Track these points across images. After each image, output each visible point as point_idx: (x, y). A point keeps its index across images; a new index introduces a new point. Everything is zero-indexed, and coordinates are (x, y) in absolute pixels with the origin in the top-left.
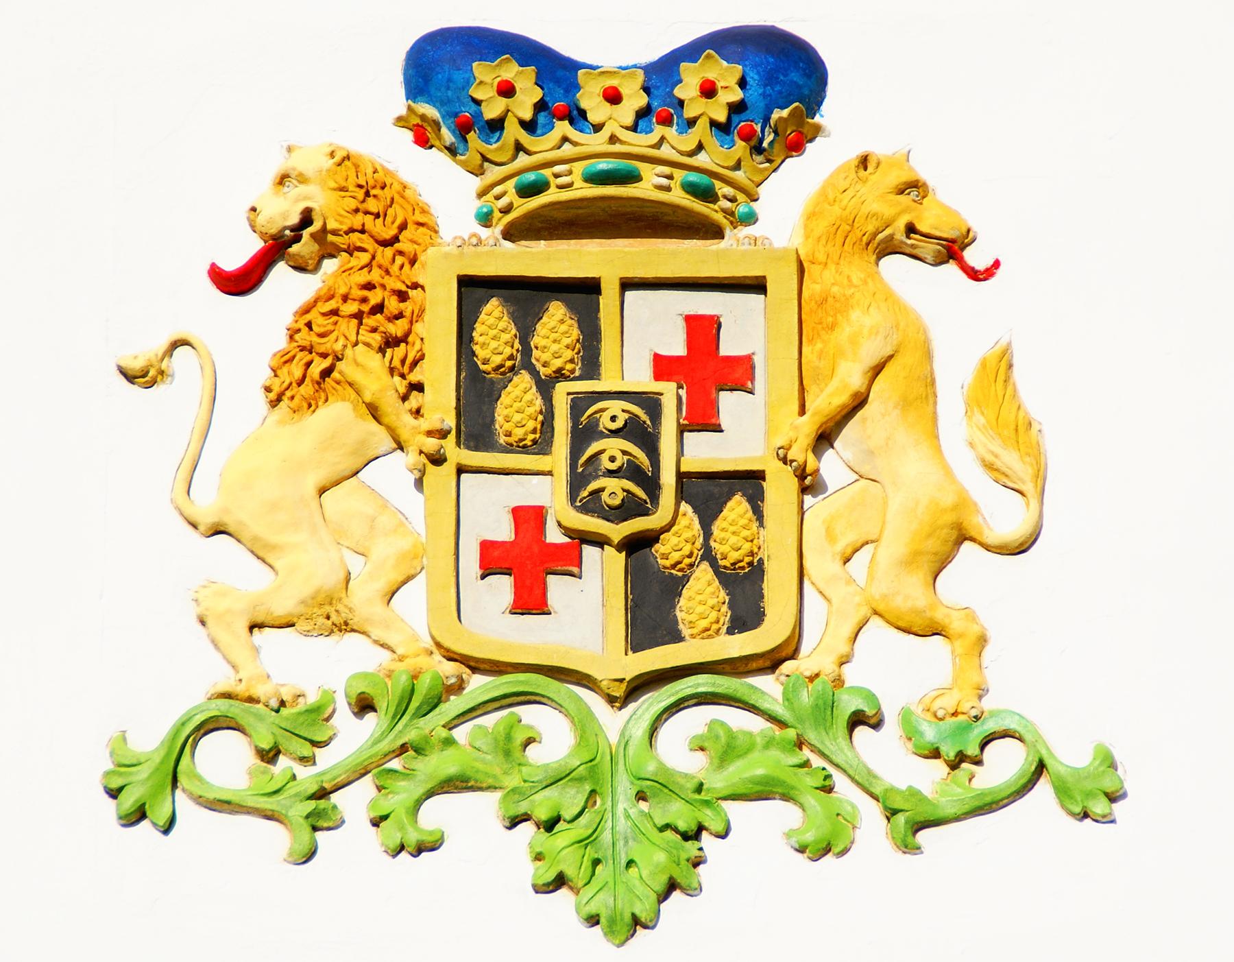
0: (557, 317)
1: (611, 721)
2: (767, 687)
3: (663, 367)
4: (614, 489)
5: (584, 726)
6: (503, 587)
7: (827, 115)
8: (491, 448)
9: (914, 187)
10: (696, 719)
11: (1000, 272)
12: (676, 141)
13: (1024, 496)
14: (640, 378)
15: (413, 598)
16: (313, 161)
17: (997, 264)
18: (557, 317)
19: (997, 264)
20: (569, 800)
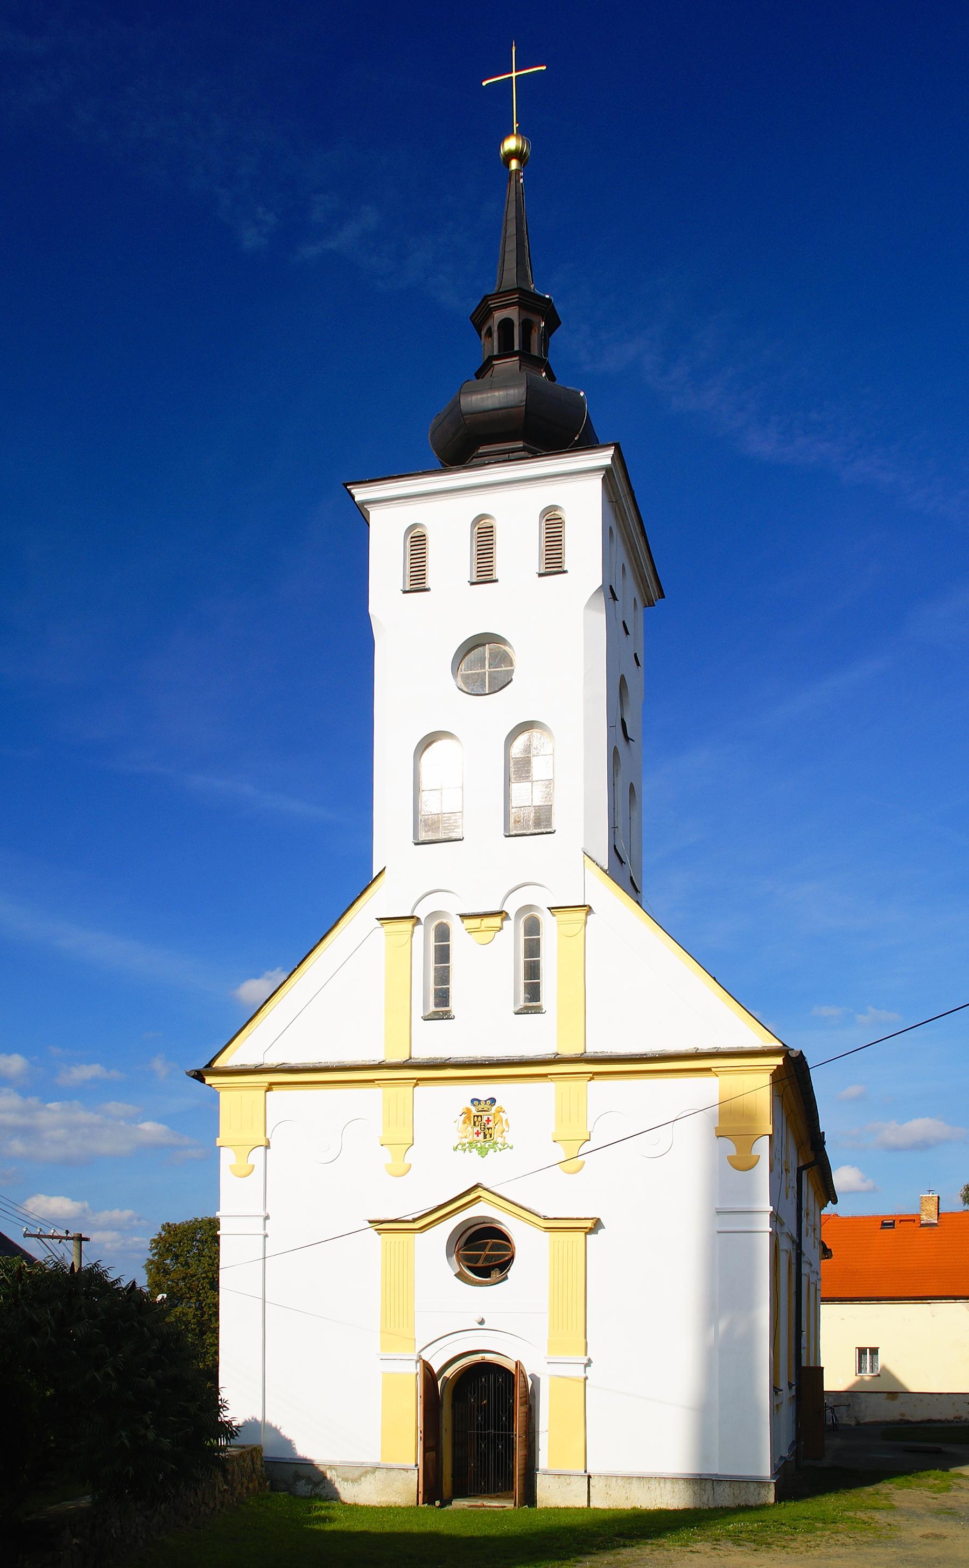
0: (480, 1118)
1: (483, 1144)
2: (492, 1141)
3: (486, 1121)
4: (483, 1129)
5: (481, 1144)
6: (476, 1135)
7: (496, 1103)
8: (697, 1509)
9: (501, 1108)
10: (488, 1144)
11: (556, 833)
12: (487, 1106)
13: (623, 720)
14: (485, 1122)
15: (471, 1136)
16: (465, 1108)
17: (555, 831)
18: (480, 1118)
19: (555, 831)
20: (480, 1149)
